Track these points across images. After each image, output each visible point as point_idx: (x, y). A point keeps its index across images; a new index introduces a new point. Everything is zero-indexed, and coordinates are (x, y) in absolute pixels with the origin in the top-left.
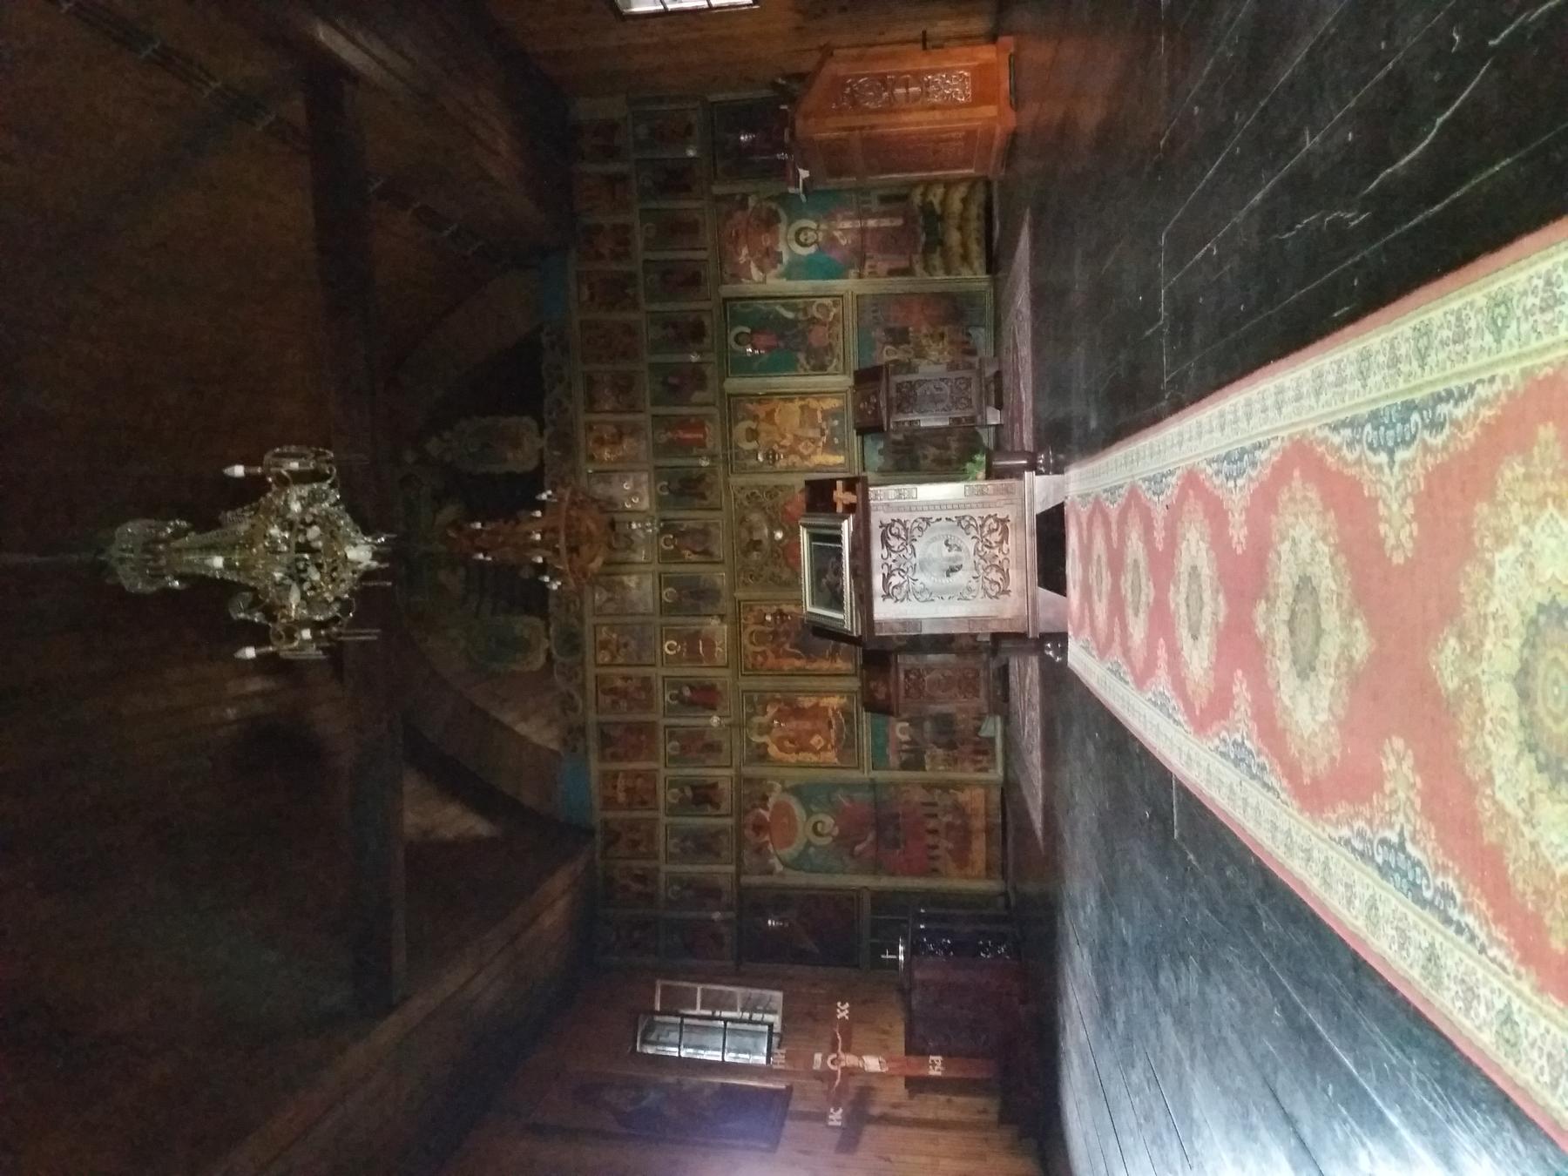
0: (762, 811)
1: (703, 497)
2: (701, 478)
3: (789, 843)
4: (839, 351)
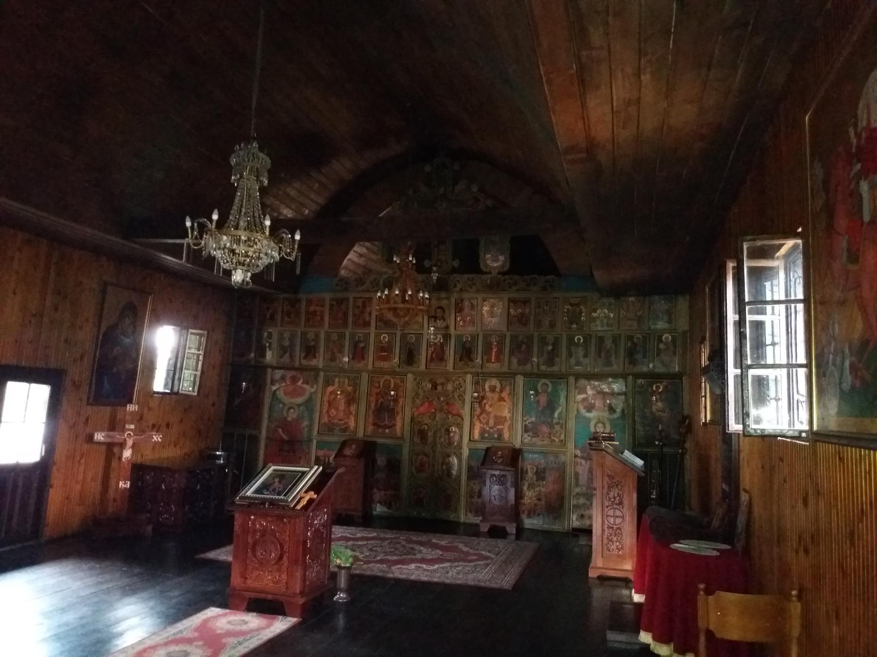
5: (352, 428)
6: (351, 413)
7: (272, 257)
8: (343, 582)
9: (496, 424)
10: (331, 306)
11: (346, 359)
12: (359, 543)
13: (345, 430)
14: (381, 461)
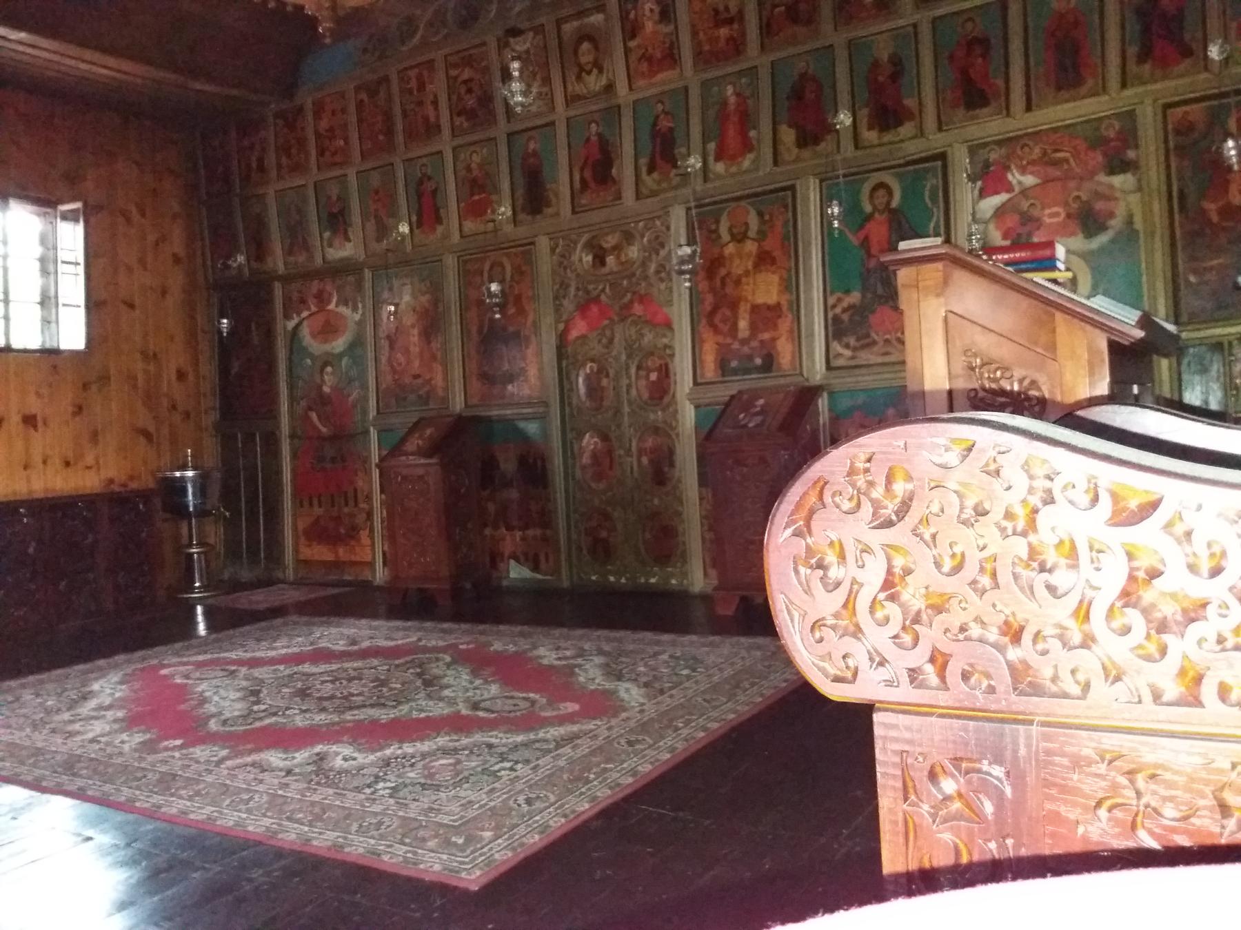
0: (335, 300)
1: (651, 169)
2: (1187, 52)
3: (313, 336)
4: (866, 357)
5: (440, 393)
6: (434, 358)
7: (409, 362)
9: (754, 328)
10: (360, 105)
11: (404, 228)
13: (425, 399)
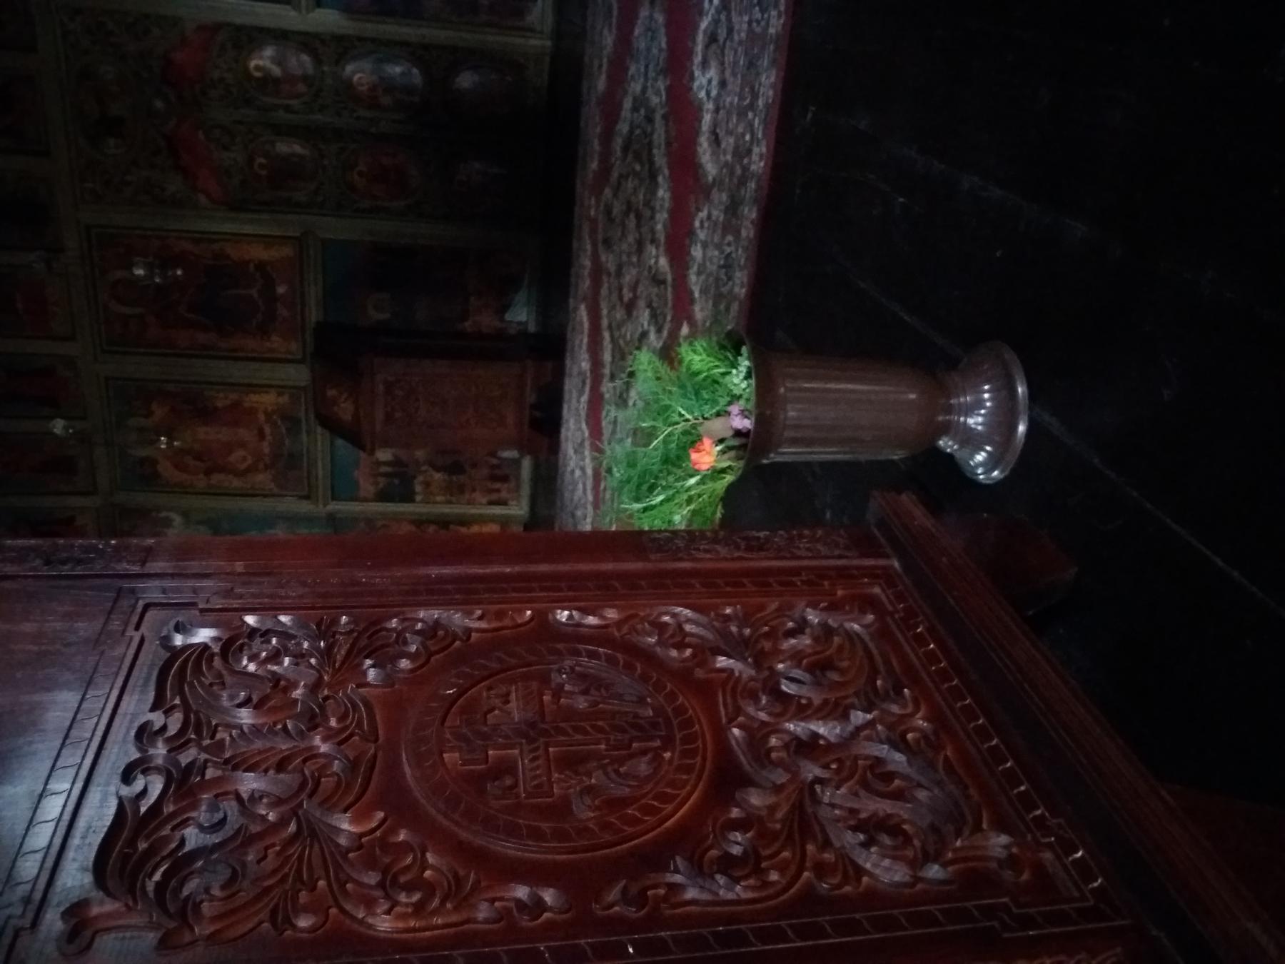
5: (284, 400)
6: (236, 405)
8: (851, 409)
12: (607, 357)
14: (376, 311)
